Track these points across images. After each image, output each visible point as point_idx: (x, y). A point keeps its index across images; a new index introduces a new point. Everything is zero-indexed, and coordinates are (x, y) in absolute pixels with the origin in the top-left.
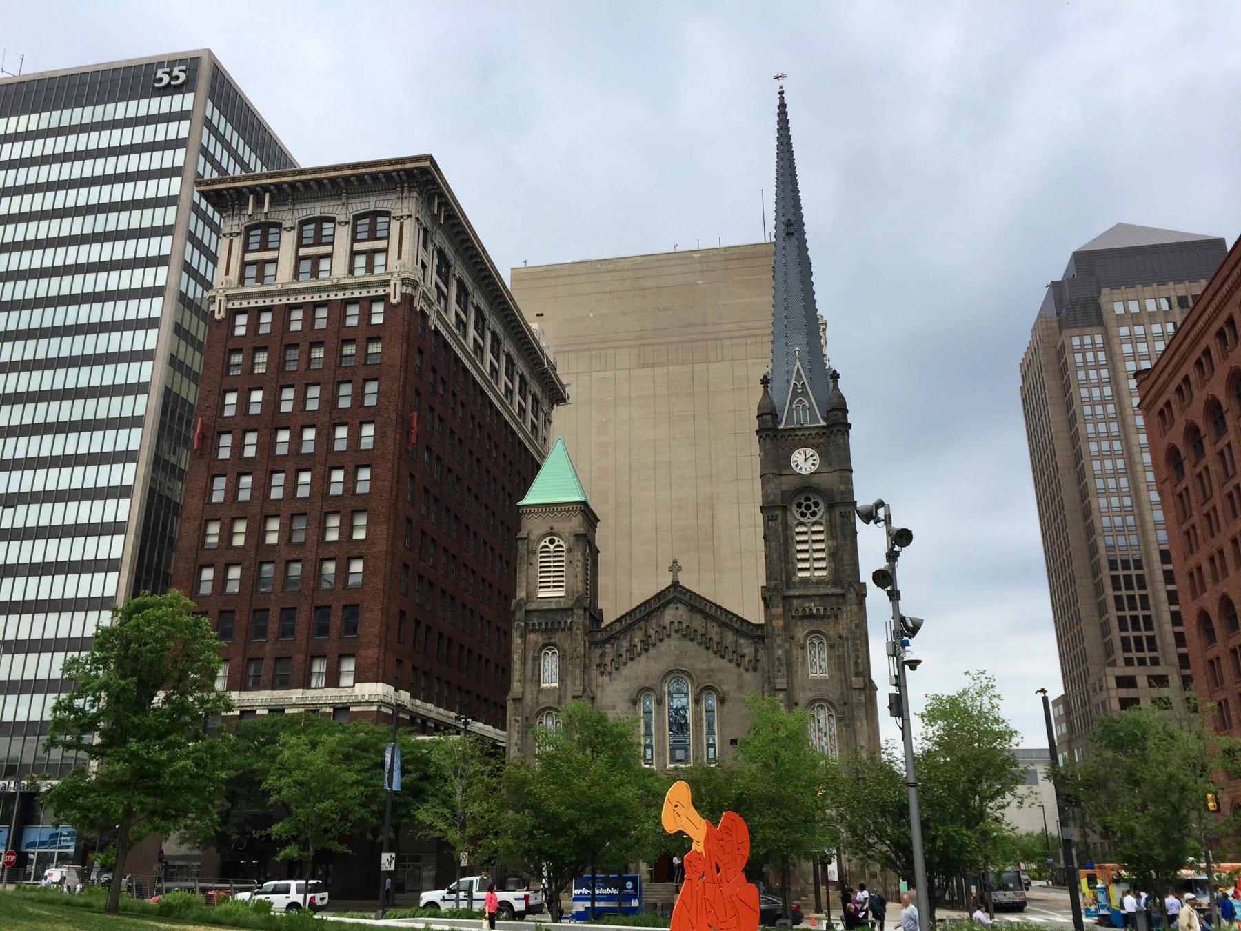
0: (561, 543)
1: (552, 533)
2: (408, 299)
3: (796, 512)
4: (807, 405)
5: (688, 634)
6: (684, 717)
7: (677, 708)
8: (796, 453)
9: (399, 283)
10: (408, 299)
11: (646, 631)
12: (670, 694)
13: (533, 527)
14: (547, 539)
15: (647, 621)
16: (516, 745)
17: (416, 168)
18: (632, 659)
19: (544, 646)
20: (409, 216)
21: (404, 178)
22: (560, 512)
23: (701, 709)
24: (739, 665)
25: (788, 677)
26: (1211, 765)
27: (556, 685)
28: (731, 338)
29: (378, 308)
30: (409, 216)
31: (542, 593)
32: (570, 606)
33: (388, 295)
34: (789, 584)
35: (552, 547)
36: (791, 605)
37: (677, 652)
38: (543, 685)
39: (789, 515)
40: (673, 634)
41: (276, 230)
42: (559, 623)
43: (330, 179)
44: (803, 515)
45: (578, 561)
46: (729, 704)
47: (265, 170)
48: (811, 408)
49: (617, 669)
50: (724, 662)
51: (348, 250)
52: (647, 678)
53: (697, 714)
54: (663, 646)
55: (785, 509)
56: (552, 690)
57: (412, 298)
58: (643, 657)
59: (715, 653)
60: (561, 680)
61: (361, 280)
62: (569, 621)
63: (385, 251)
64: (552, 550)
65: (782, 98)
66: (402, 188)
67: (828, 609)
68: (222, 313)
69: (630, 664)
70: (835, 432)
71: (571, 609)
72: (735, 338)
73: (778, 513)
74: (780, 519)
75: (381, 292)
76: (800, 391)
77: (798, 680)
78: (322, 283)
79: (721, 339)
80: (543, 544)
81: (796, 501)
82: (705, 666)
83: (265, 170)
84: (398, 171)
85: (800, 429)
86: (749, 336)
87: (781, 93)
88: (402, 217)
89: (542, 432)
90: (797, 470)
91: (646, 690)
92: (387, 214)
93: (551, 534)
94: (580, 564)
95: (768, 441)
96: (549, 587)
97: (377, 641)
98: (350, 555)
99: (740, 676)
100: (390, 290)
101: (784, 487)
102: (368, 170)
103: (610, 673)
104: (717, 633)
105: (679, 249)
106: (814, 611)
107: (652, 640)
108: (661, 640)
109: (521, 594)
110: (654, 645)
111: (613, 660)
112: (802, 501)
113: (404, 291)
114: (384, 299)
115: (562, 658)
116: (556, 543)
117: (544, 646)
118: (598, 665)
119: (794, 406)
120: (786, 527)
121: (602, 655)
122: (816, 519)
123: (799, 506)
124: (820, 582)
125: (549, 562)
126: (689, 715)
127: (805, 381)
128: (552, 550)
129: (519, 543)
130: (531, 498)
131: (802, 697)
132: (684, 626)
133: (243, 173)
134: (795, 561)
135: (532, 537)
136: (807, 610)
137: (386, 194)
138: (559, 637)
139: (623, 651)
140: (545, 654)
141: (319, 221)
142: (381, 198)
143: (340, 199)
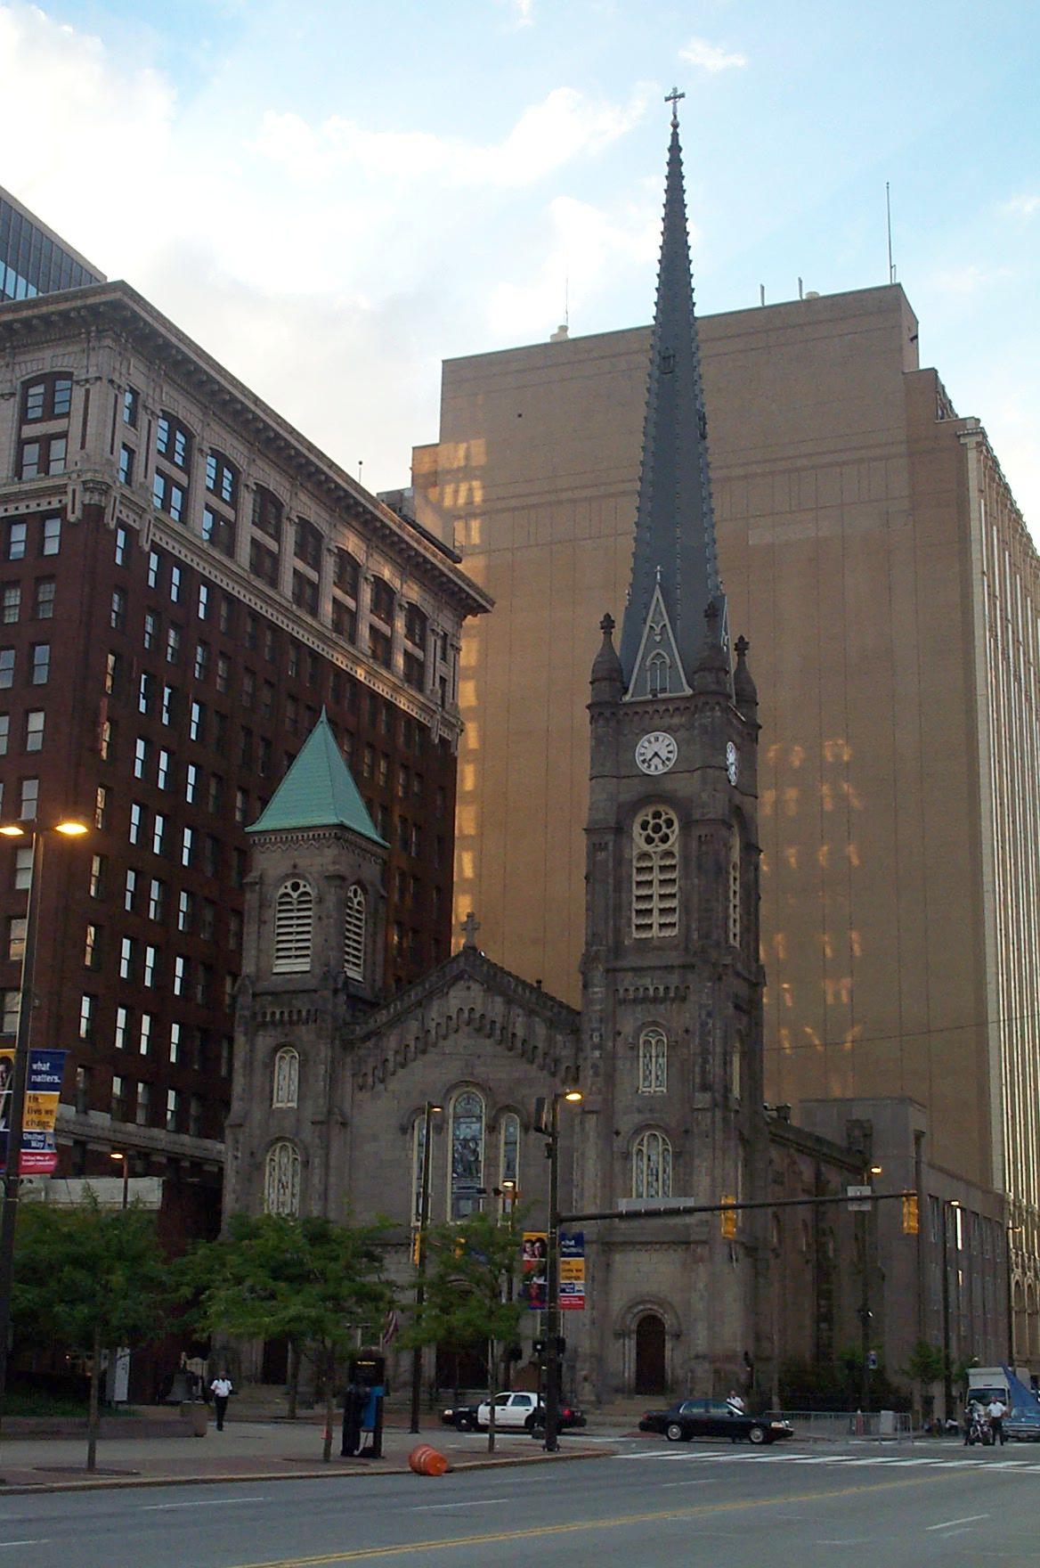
0: (308, 889)
1: (295, 873)
2: (94, 514)
4: (668, 661)
5: (482, 1026)
6: (475, 1152)
7: (464, 1139)
9: (79, 488)
13: (269, 863)
14: (289, 884)
16: (234, 1192)
17: (105, 303)
18: (403, 1066)
20: (99, 378)
22: (284, 843)
23: (498, 1141)
24: (553, 1074)
27: (294, 1105)
29: (53, 528)
30: (99, 378)
31: (282, 966)
33: (64, 508)
34: (618, 950)
35: (295, 895)
38: (276, 1105)
41: (67, 384)
43: (42, 318)
47: (33, 293)
48: (673, 666)
51: (14, 437)
53: (492, 1146)
54: (448, 1045)
57: (100, 511)
61: (35, 486)
63: (64, 435)
66: (89, 333)
68: (78, 513)
69: (401, 1072)
70: (700, 705)
73: (610, 838)
75: (55, 505)
76: (658, 638)
78: (26, 487)
80: (282, 890)
81: (639, 819)
83: (33, 293)
84: (78, 309)
88: (87, 381)
89: (435, 669)
92: (68, 376)
93: (294, 875)
95: (601, 722)
100: (68, 499)
101: (624, 797)
102: (36, 312)
106: (651, 992)
108: (445, 1037)
109: (248, 968)
110: (435, 1045)
112: (649, 818)
113: (86, 502)
114: (59, 513)
116: (302, 889)
120: (620, 861)
122: (665, 846)
123: (657, 815)
126: (481, 1149)
127: (667, 622)
130: (270, 820)
131: (626, 1123)
132: (477, 1016)
133: (41, 294)
137: (68, 344)
140: (282, 1058)
141: (49, 379)
142: (60, 351)
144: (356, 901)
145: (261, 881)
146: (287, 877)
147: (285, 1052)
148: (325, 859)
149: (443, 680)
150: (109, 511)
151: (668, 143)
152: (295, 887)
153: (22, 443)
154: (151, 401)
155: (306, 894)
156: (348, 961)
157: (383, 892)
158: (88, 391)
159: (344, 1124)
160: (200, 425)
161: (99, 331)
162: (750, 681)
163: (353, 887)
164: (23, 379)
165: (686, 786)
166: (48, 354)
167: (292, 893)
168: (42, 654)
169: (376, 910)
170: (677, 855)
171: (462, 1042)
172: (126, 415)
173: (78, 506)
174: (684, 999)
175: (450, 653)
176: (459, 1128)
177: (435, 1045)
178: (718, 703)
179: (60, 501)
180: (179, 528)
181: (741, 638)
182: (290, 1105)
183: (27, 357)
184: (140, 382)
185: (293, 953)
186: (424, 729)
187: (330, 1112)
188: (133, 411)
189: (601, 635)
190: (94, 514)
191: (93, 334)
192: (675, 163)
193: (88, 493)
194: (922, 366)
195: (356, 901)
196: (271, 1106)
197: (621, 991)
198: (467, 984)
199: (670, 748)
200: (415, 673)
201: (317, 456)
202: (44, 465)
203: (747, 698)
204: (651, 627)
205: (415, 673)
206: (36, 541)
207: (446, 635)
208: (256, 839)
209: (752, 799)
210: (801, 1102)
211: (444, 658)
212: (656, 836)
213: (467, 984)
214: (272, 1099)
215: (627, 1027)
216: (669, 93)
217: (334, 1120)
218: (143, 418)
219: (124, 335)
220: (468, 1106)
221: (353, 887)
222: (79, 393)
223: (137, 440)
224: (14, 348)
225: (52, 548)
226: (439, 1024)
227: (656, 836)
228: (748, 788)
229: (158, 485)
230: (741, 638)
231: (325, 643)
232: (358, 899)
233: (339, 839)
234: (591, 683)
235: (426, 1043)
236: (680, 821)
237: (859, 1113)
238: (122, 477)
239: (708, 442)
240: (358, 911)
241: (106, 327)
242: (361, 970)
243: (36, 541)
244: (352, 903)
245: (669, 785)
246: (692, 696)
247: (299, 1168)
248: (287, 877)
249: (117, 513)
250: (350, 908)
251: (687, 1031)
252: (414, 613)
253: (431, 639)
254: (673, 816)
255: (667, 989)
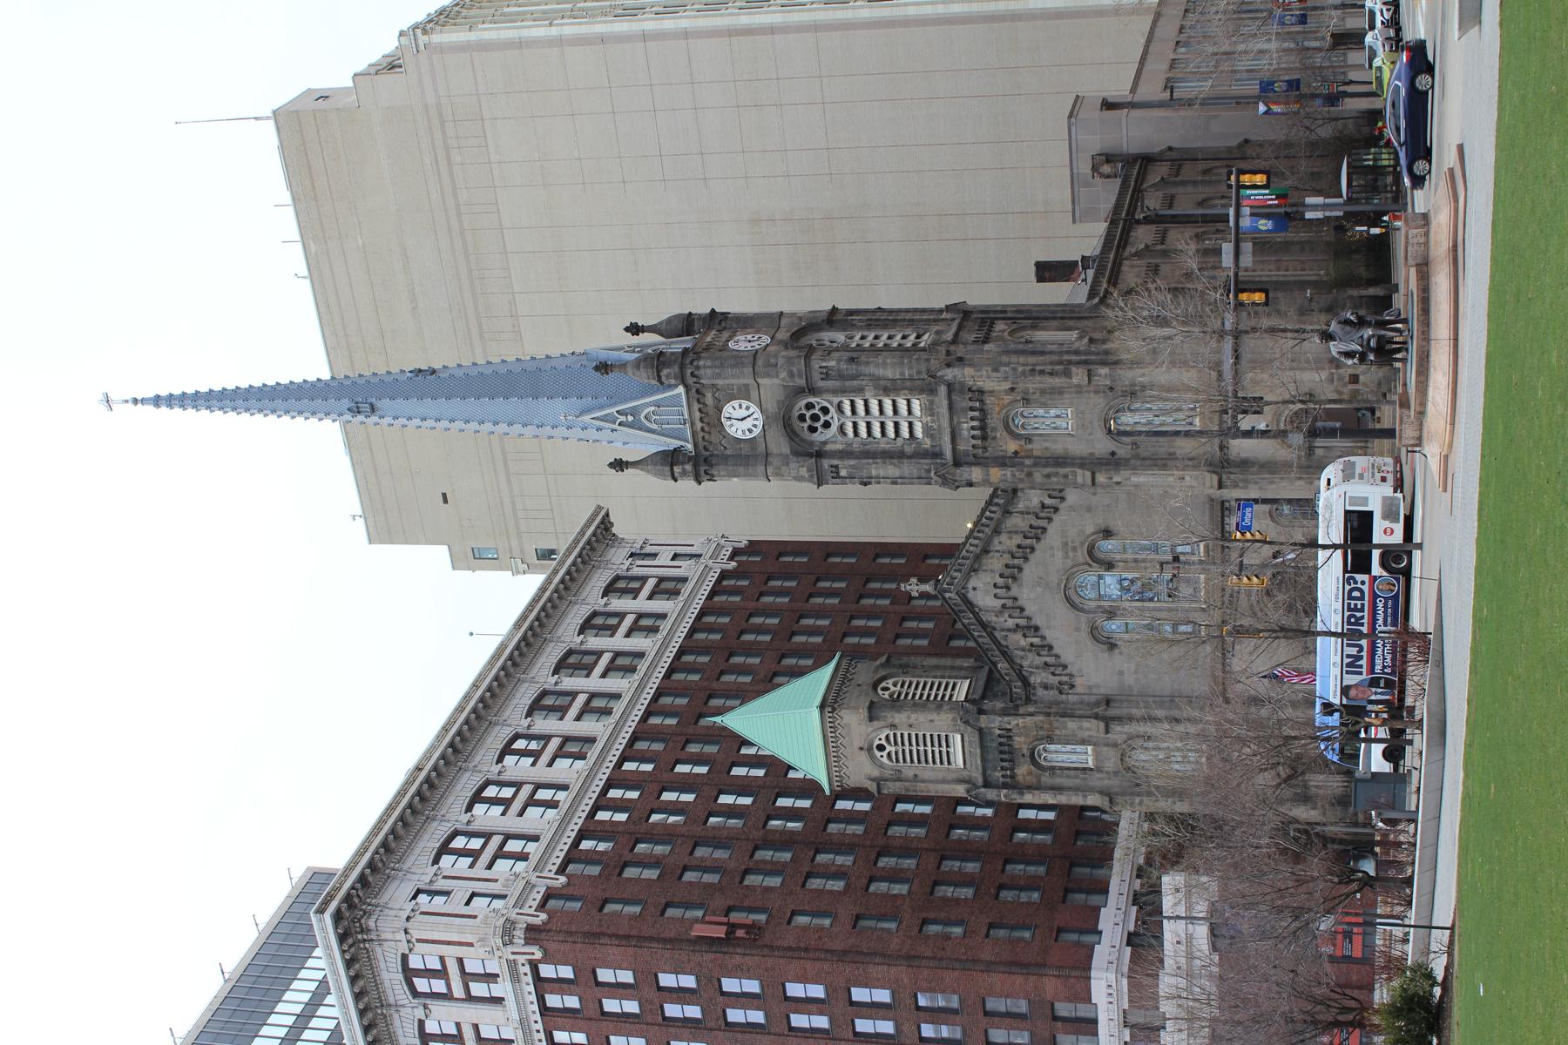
0: (883, 736)
2: (534, 934)
3: (820, 436)
4: (652, 408)
5: (1012, 574)
6: (1132, 581)
8: (731, 431)
9: (510, 949)
10: (533, 935)
11: (1009, 630)
12: (1100, 597)
13: (859, 771)
14: (878, 754)
15: (994, 629)
18: (1050, 648)
19: (1034, 761)
21: (350, 941)
24: (1056, 509)
25: (1073, 465)
26: (1266, 779)
28: (454, 189)
29: (547, 971)
30: (406, 932)
32: (977, 734)
35: (888, 748)
36: (966, 454)
37: (1038, 589)
39: (829, 447)
40: (1011, 594)
42: (1001, 744)
44: (827, 425)
45: (909, 717)
46: (1117, 524)
49: (1065, 667)
50: (1052, 529)
51: (466, 1005)
52: (1077, 629)
55: (819, 455)
56: (1097, 755)
57: (530, 929)
58: (1047, 633)
59: (1038, 539)
60: (1083, 742)
62: (999, 732)
63: (460, 961)
64: (893, 749)
65: (143, 401)
67: (971, 404)
69: (1056, 650)
71: (980, 730)
72: (453, 182)
73: (826, 463)
74: (835, 462)
75: (527, 969)
77: (1078, 448)
79: (458, 206)
80: (885, 760)
81: (806, 435)
82: (1059, 554)
85: (692, 424)
86: (449, 159)
87: (135, 401)
88: (408, 942)
90: (756, 432)
91: (1094, 633)
92: (405, 958)
93: (870, 749)
94: (914, 716)
96: (948, 752)
97: (1032, 979)
98: (913, 1007)
99: (1072, 508)
101: (786, 449)
103: (1071, 676)
104: (1011, 538)
105: (305, 272)
106: (975, 423)
107: (1022, 622)
108: (1022, 609)
111: (1053, 674)
112: (806, 425)
113: (523, 942)
114: (534, 966)
115: (1050, 740)
116: (883, 742)
117: (1034, 761)
118: (1061, 693)
119: (654, 426)
120: (845, 454)
121: (1046, 687)
123: (813, 430)
124: (929, 410)
125: (911, 751)
127: (613, 410)
128: (893, 749)
129: (885, 792)
134: (900, 442)
135: (876, 773)
136: (973, 432)
138: (1020, 742)
139: (1039, 661)
141: (409, 974)
142: (382, 965)
143: (391, 1015)
144: (893, 689)
145: (878, 781)
146: (872, 757)
147: (1040, 756)
148: (853, 720)
149: (675, 557)
150: (531, 920)
151: (150, 408)
152: (881, 748)
153: (470, 998)
154: (423, 877)
155: (887, 737)
156: (951, 696)
157: (883, 659)
158: (419, 941)
159: (1108, 702)
160: (443, 823)
161: (362, 931)
162: (669, 320)
163: (880, 692)
164: (410, 997)
165: (772, 387)
166: (385, 976)
167: (887, 751)
168: (667, 980)
169: (901, 666)
170: (840, 399)
171: (1026, 594)
172: (439, 900)
173: (527, 949)
174: (981, 392)
175: (648, 549)
176: (1110, 596)
177: (1029, 618)
178: (691, 363)
179: (523, 965)
180: (544, 842)
181: (627, 329)
182: (1090, 752)
183: (389, 992)
184: (409, 889)
185: (944, 749)
186: (724, 575)
187: (1096, 717)
188: (433, 893)
189: (629, 471)
190: (534, 934)
191: (365, 937)
192: (170, 401)
193: (515, 941)
194: (351, 85)
195: (893, 689)
196: (1092, 769)
197: (976, 451)
198: (971, 591)
199: (737, 406)
200: (667, 588)
201: (468, 702)
202: (491, 978)
203: (686, 324)
204: (619, 424)
205: (667, 588)
206: (560, 985)
207: (632, 555)
208: (836, 784)
209: (782, 318)
210: (1074, 222)
211: (654, 555)
212: (823, 419)
213: (971, 591)
214: (1084, 769)
215: (1012, 446)
216: (103, 408)
217: (1106, 710)
218: (441, 884)
219: (364, 907)
220: (1089, 587)
221: (880, 692)
222: (419, 947)
223: (462, 890)
224: (382, 1006)
225: (566, 972)
226: (1010, 616)
227: (823, 419)
228: (770, 321)
229: (503, 865)
230: (627, 329)
231: (645, 687)
232: (890, 686)
233: (834, 709)
234: (676, 481)
235: (1029, 627)
236: (807, 397)
237: (1085, 168)
238: (497, 904)
239: (437, 366)
240: (902, 686)
241: (357, 925)
242: (959, 682)
243: (560, 985)
244: (894, 693)
245: (772, 407)
246: (686, 386)
247: (1151, 744)
248: (872, 757)
249: (532, 911)
250: (899, 695)
251: (1012, 389)
252: (616, 587)
253: (636, 571)
254: (803, 403)
255: (972, 409)
